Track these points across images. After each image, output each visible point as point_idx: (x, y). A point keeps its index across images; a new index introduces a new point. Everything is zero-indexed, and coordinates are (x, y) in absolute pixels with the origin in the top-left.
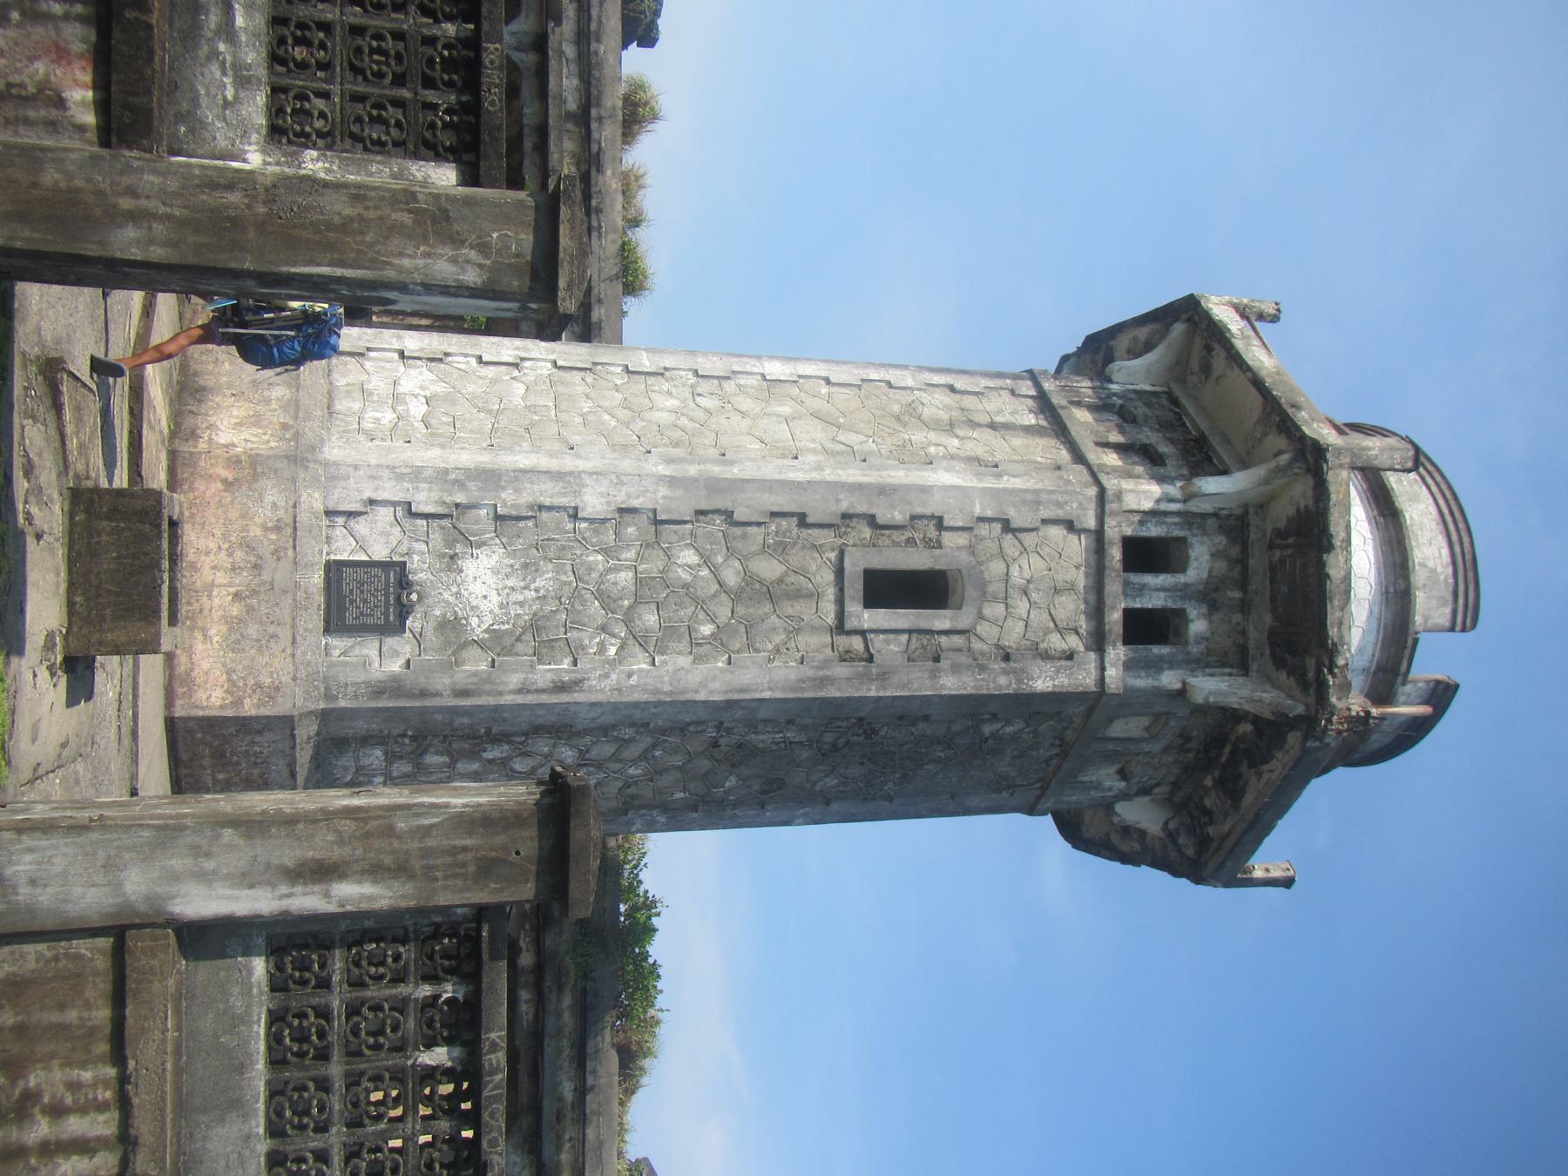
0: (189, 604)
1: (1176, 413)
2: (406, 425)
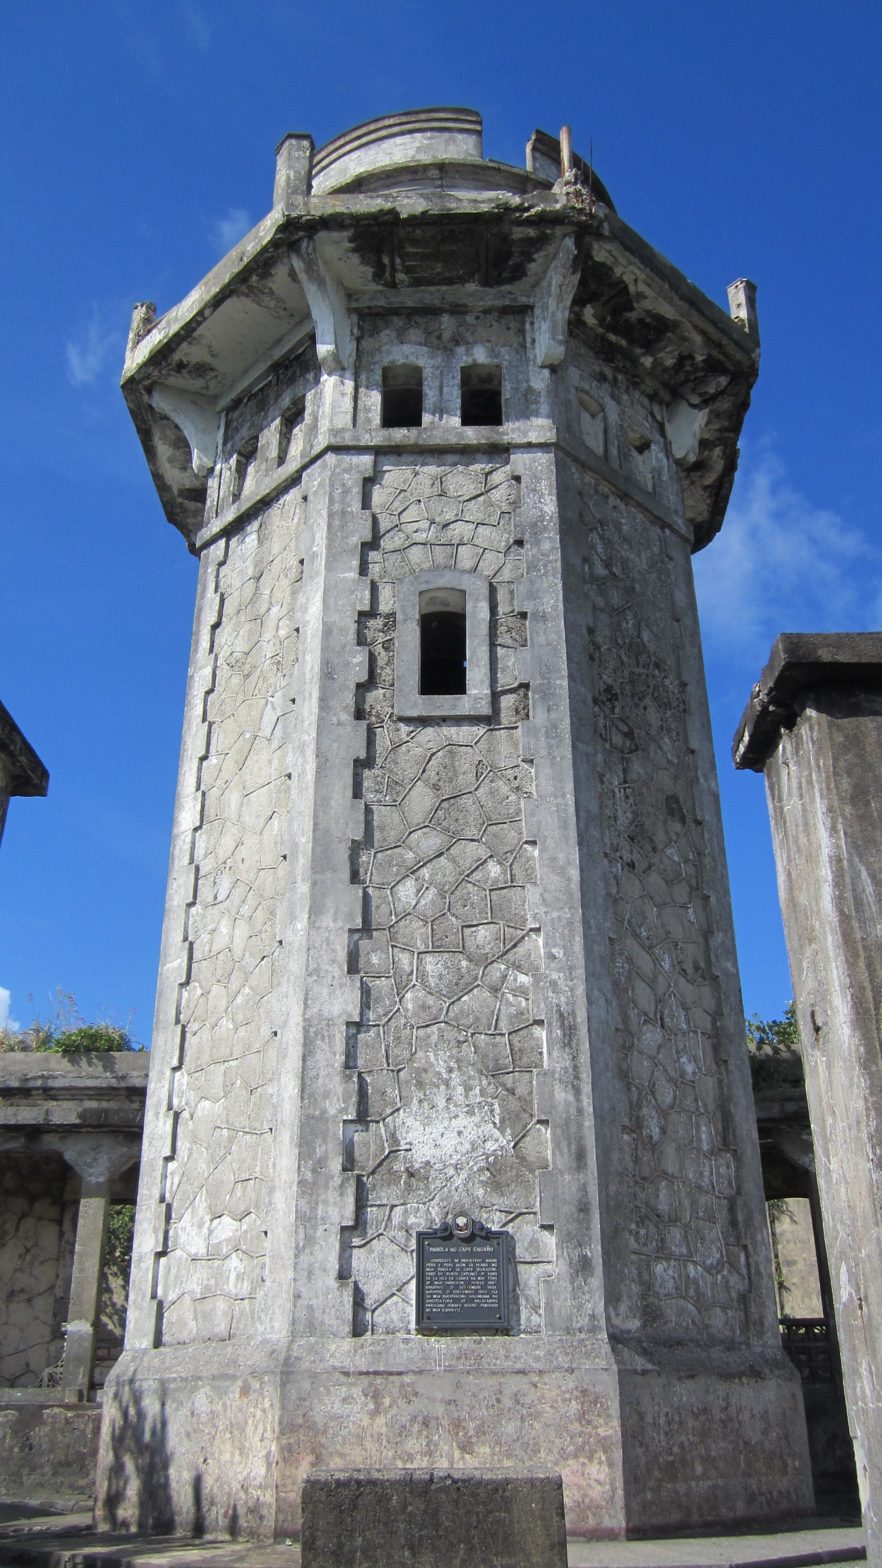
1: (249, 400)
2: (245, 1240)
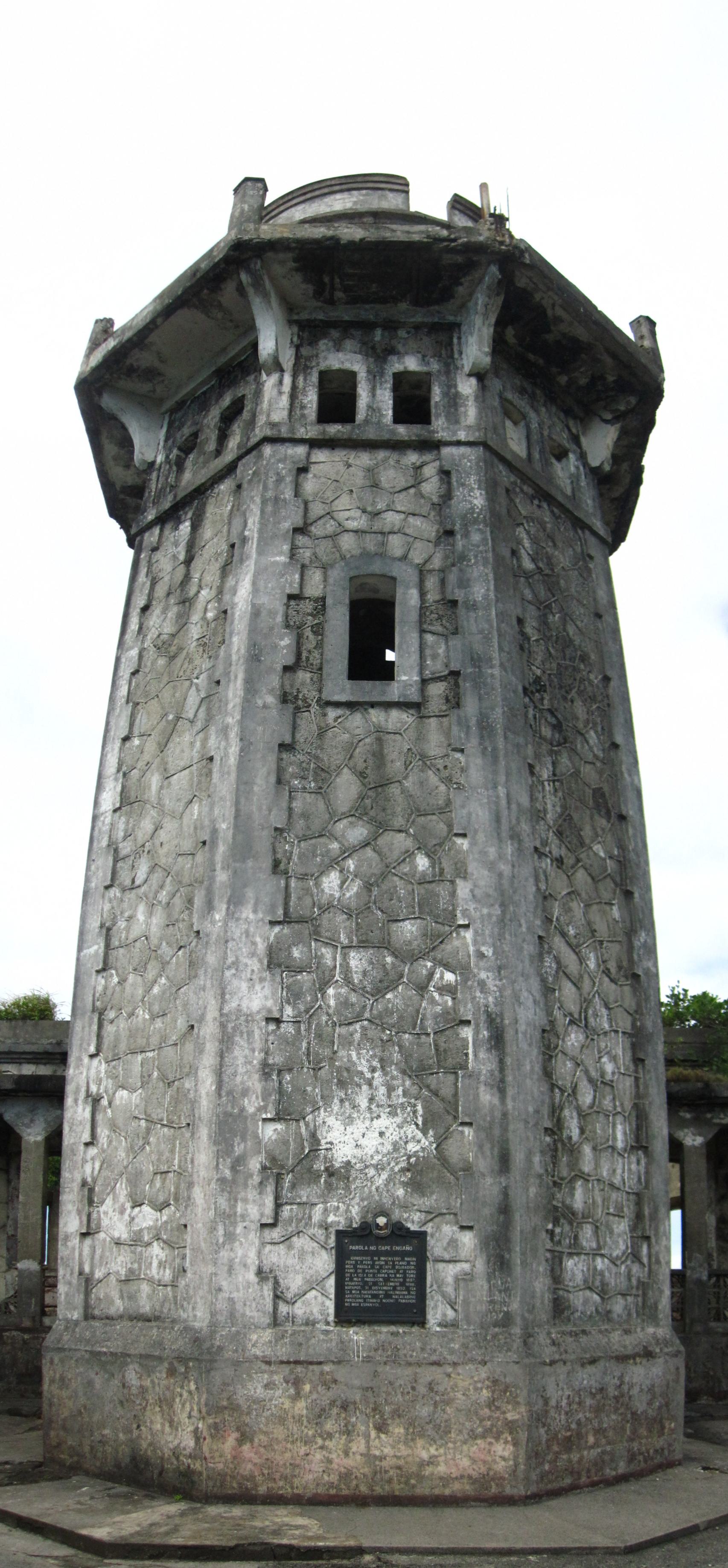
0: (390, 1481)
1: (192, 402)
